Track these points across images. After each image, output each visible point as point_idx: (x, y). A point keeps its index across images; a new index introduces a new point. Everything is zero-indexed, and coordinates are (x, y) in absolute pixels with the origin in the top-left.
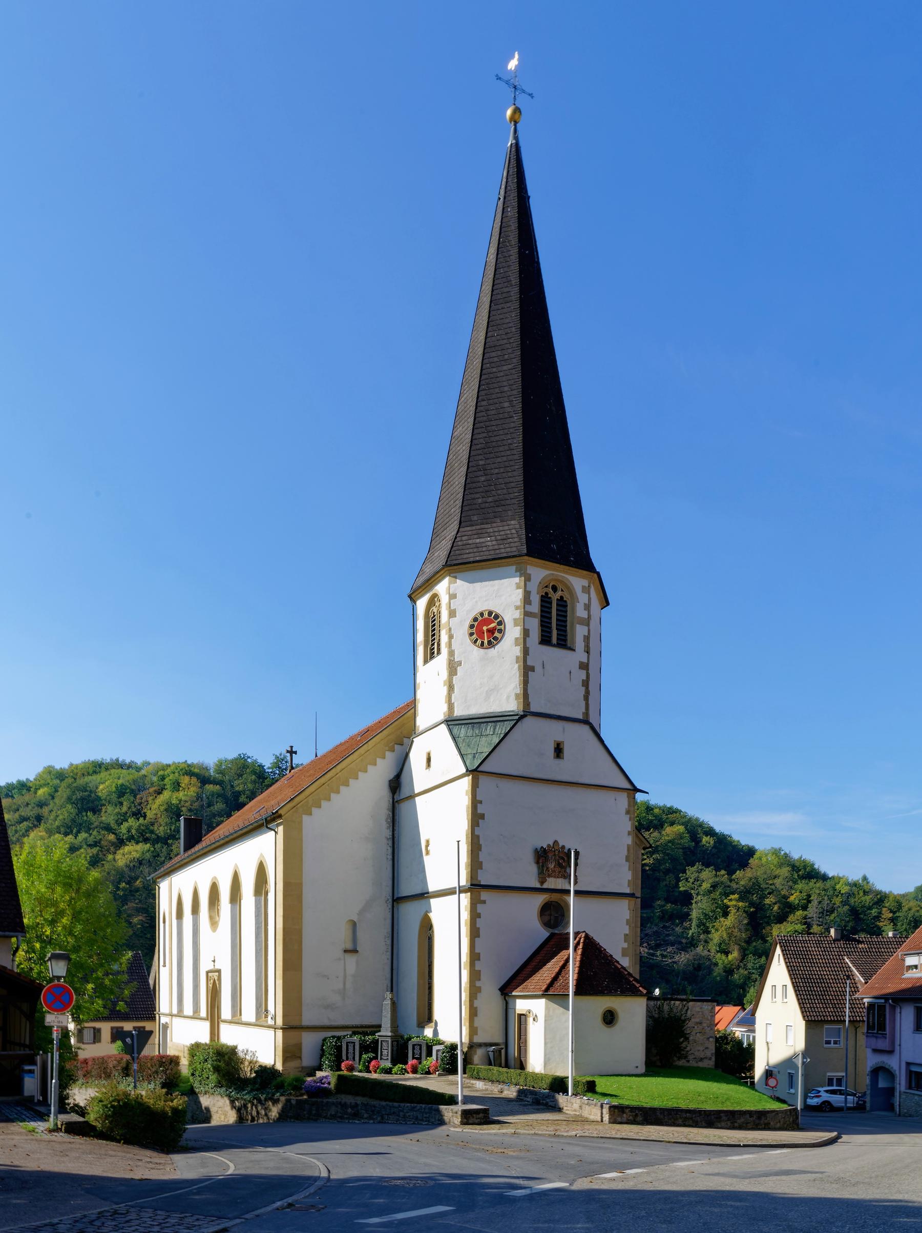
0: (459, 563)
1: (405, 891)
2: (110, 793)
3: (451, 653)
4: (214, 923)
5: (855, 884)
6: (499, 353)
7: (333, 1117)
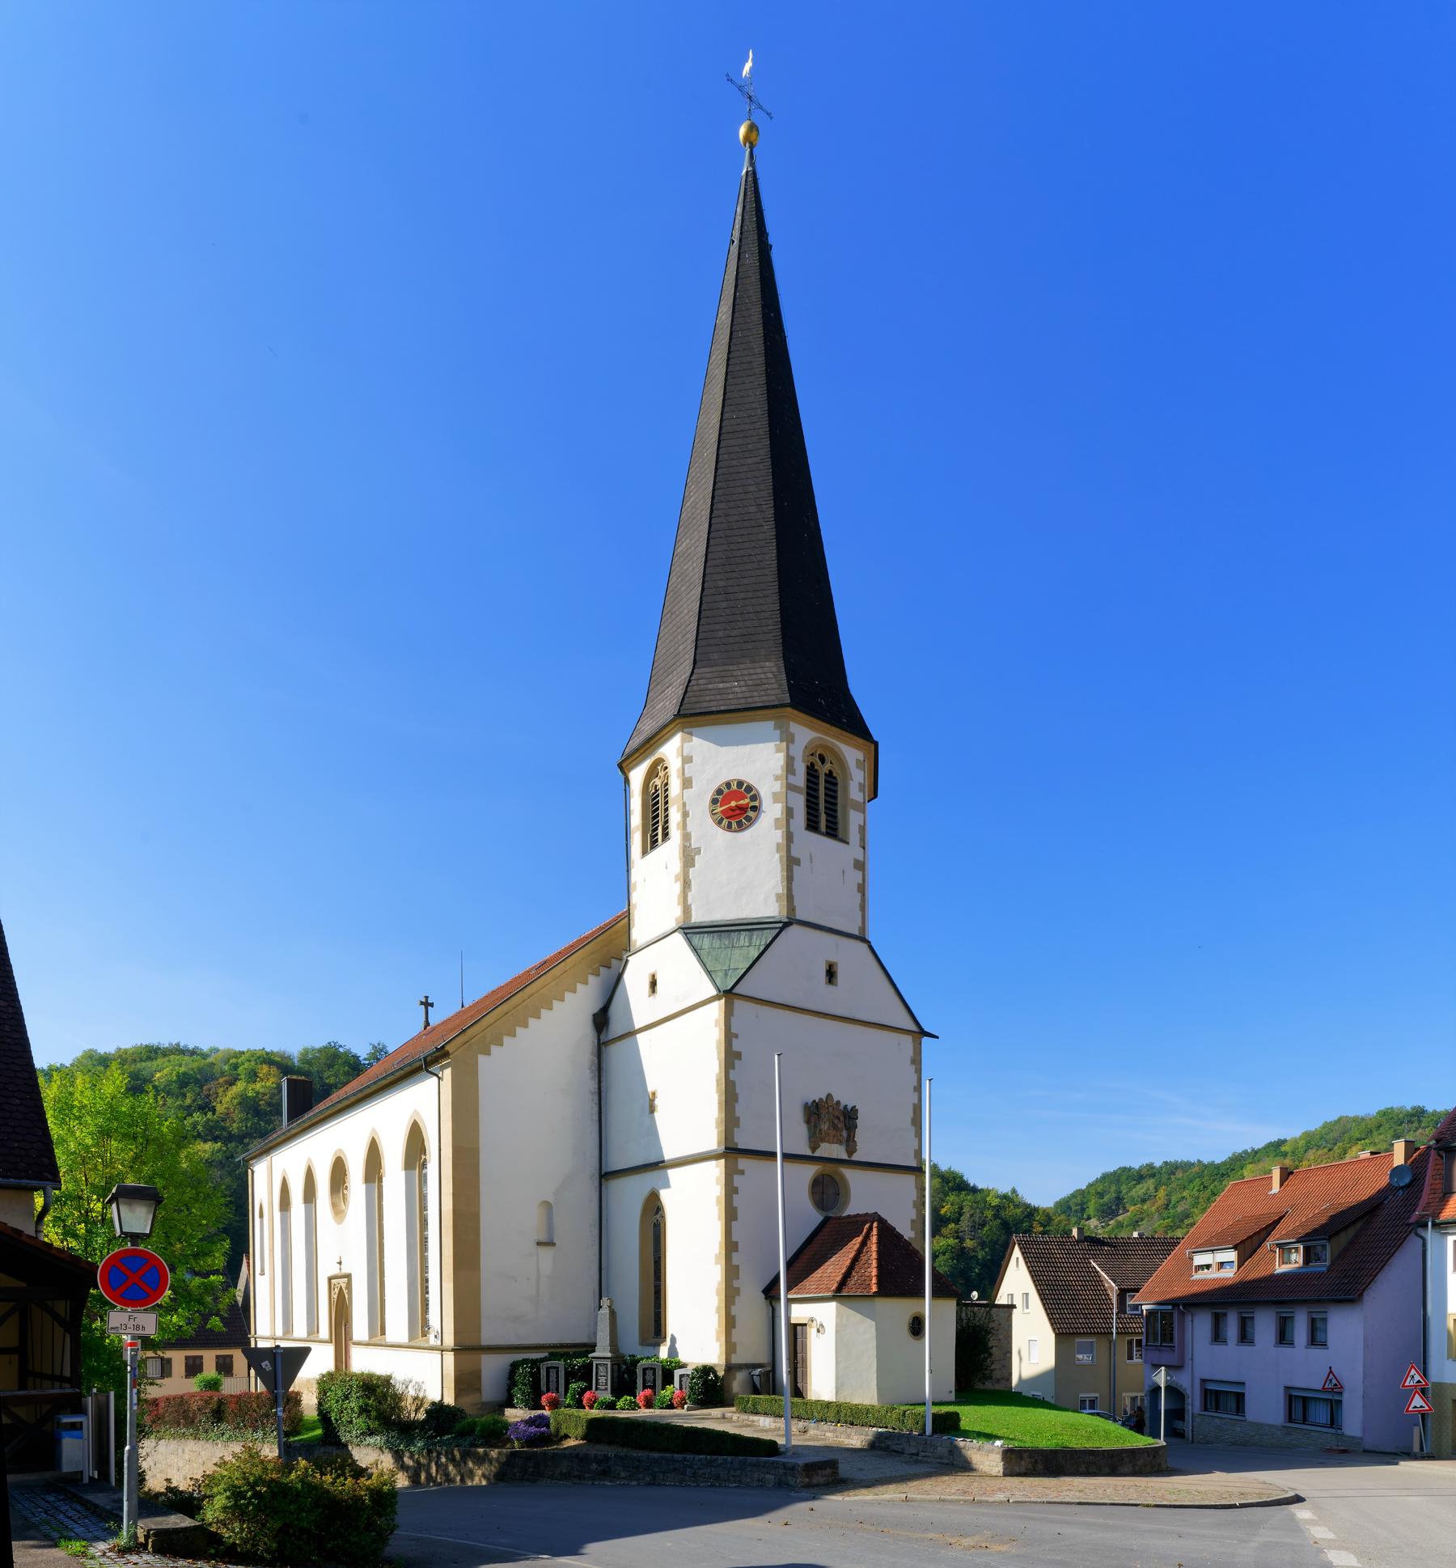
0: (693, 714)
1: (616, 1162)
2: (170, 1083)
3: (686, 837)
4: (338, 1212)
5: (1005, 1197)
6: (741, 441)
7: (566, 1476)
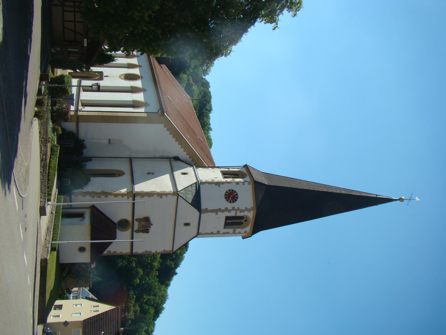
3: (223, 183)
